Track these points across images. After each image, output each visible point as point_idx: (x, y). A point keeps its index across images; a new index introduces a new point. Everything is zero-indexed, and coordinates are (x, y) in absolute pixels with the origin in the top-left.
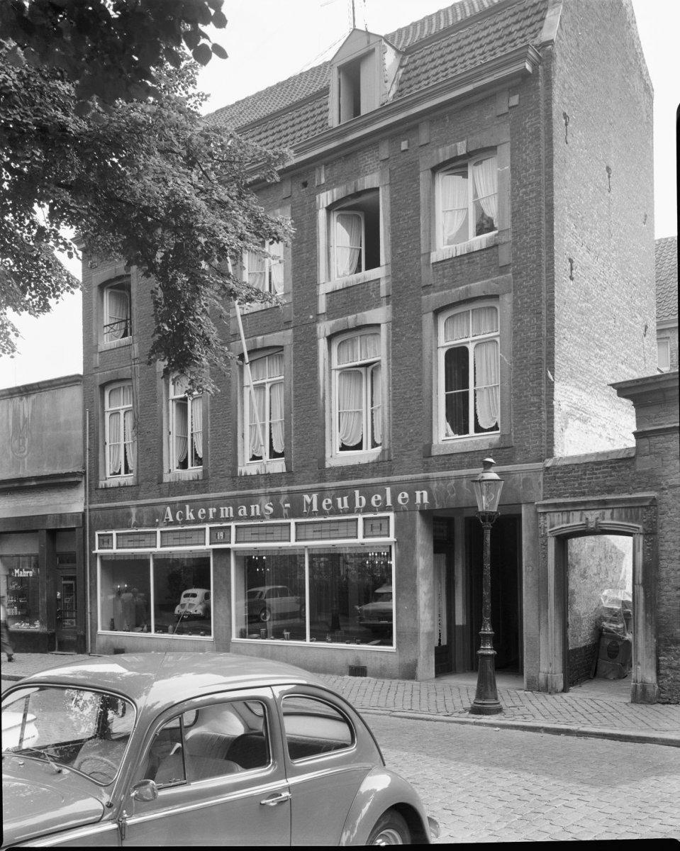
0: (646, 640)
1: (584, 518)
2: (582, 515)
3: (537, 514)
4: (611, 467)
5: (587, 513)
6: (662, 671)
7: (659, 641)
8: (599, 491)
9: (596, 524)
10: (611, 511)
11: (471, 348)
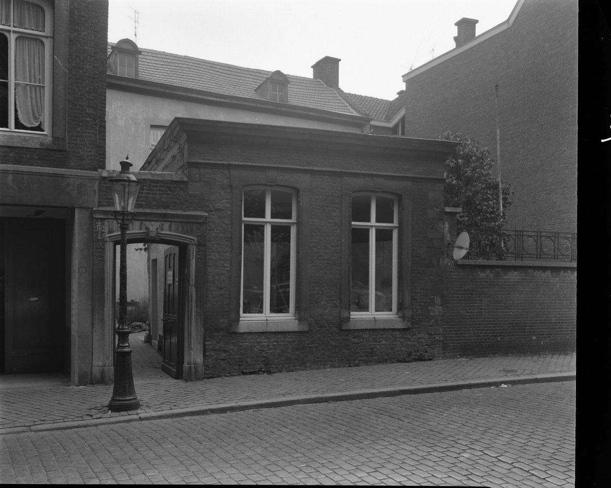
0: (197, 330)
1: (143, 227)
2: (141, 224)
3: (91, 218)
4: (167, 187)
5: (147, 223)
6: (208, 354)
7: (205, 329)
8: (156, 205)
9: (157, 233)
10: (169, 223)
11: (12, 39)
